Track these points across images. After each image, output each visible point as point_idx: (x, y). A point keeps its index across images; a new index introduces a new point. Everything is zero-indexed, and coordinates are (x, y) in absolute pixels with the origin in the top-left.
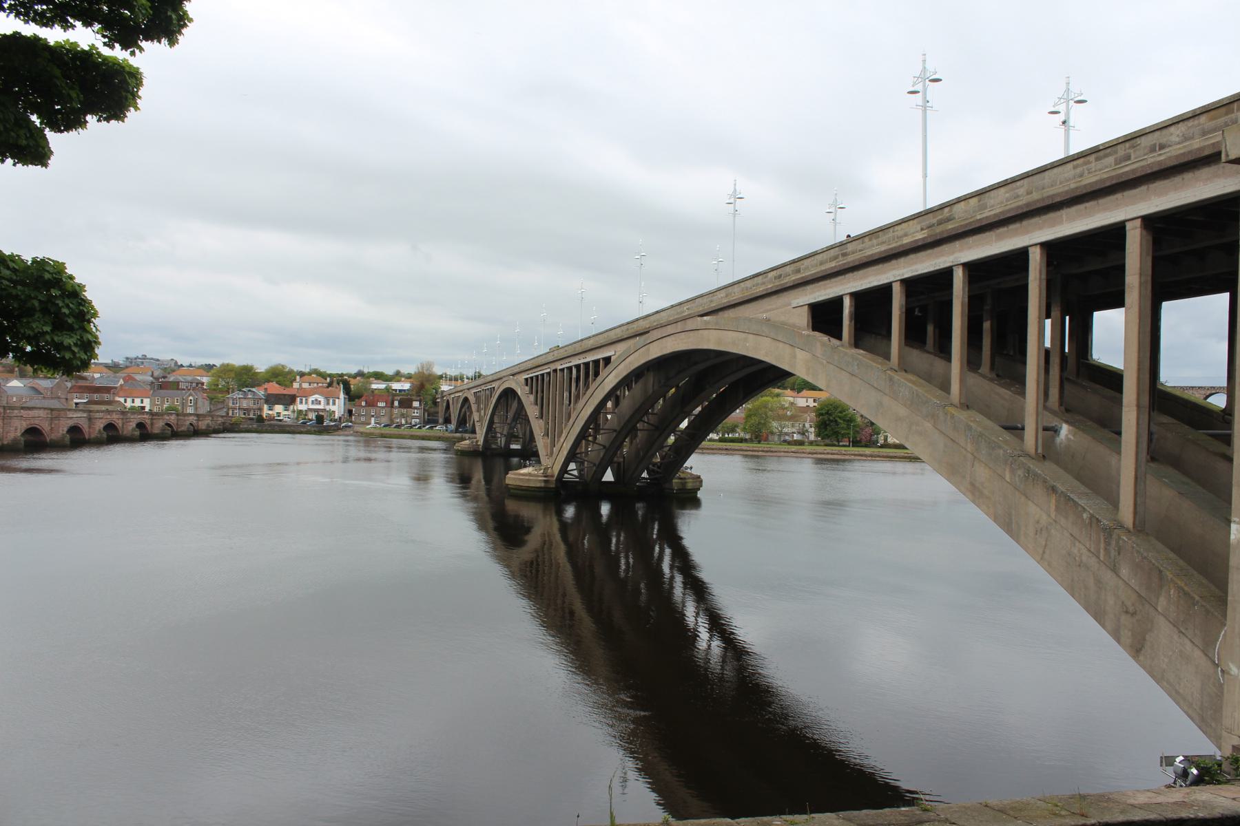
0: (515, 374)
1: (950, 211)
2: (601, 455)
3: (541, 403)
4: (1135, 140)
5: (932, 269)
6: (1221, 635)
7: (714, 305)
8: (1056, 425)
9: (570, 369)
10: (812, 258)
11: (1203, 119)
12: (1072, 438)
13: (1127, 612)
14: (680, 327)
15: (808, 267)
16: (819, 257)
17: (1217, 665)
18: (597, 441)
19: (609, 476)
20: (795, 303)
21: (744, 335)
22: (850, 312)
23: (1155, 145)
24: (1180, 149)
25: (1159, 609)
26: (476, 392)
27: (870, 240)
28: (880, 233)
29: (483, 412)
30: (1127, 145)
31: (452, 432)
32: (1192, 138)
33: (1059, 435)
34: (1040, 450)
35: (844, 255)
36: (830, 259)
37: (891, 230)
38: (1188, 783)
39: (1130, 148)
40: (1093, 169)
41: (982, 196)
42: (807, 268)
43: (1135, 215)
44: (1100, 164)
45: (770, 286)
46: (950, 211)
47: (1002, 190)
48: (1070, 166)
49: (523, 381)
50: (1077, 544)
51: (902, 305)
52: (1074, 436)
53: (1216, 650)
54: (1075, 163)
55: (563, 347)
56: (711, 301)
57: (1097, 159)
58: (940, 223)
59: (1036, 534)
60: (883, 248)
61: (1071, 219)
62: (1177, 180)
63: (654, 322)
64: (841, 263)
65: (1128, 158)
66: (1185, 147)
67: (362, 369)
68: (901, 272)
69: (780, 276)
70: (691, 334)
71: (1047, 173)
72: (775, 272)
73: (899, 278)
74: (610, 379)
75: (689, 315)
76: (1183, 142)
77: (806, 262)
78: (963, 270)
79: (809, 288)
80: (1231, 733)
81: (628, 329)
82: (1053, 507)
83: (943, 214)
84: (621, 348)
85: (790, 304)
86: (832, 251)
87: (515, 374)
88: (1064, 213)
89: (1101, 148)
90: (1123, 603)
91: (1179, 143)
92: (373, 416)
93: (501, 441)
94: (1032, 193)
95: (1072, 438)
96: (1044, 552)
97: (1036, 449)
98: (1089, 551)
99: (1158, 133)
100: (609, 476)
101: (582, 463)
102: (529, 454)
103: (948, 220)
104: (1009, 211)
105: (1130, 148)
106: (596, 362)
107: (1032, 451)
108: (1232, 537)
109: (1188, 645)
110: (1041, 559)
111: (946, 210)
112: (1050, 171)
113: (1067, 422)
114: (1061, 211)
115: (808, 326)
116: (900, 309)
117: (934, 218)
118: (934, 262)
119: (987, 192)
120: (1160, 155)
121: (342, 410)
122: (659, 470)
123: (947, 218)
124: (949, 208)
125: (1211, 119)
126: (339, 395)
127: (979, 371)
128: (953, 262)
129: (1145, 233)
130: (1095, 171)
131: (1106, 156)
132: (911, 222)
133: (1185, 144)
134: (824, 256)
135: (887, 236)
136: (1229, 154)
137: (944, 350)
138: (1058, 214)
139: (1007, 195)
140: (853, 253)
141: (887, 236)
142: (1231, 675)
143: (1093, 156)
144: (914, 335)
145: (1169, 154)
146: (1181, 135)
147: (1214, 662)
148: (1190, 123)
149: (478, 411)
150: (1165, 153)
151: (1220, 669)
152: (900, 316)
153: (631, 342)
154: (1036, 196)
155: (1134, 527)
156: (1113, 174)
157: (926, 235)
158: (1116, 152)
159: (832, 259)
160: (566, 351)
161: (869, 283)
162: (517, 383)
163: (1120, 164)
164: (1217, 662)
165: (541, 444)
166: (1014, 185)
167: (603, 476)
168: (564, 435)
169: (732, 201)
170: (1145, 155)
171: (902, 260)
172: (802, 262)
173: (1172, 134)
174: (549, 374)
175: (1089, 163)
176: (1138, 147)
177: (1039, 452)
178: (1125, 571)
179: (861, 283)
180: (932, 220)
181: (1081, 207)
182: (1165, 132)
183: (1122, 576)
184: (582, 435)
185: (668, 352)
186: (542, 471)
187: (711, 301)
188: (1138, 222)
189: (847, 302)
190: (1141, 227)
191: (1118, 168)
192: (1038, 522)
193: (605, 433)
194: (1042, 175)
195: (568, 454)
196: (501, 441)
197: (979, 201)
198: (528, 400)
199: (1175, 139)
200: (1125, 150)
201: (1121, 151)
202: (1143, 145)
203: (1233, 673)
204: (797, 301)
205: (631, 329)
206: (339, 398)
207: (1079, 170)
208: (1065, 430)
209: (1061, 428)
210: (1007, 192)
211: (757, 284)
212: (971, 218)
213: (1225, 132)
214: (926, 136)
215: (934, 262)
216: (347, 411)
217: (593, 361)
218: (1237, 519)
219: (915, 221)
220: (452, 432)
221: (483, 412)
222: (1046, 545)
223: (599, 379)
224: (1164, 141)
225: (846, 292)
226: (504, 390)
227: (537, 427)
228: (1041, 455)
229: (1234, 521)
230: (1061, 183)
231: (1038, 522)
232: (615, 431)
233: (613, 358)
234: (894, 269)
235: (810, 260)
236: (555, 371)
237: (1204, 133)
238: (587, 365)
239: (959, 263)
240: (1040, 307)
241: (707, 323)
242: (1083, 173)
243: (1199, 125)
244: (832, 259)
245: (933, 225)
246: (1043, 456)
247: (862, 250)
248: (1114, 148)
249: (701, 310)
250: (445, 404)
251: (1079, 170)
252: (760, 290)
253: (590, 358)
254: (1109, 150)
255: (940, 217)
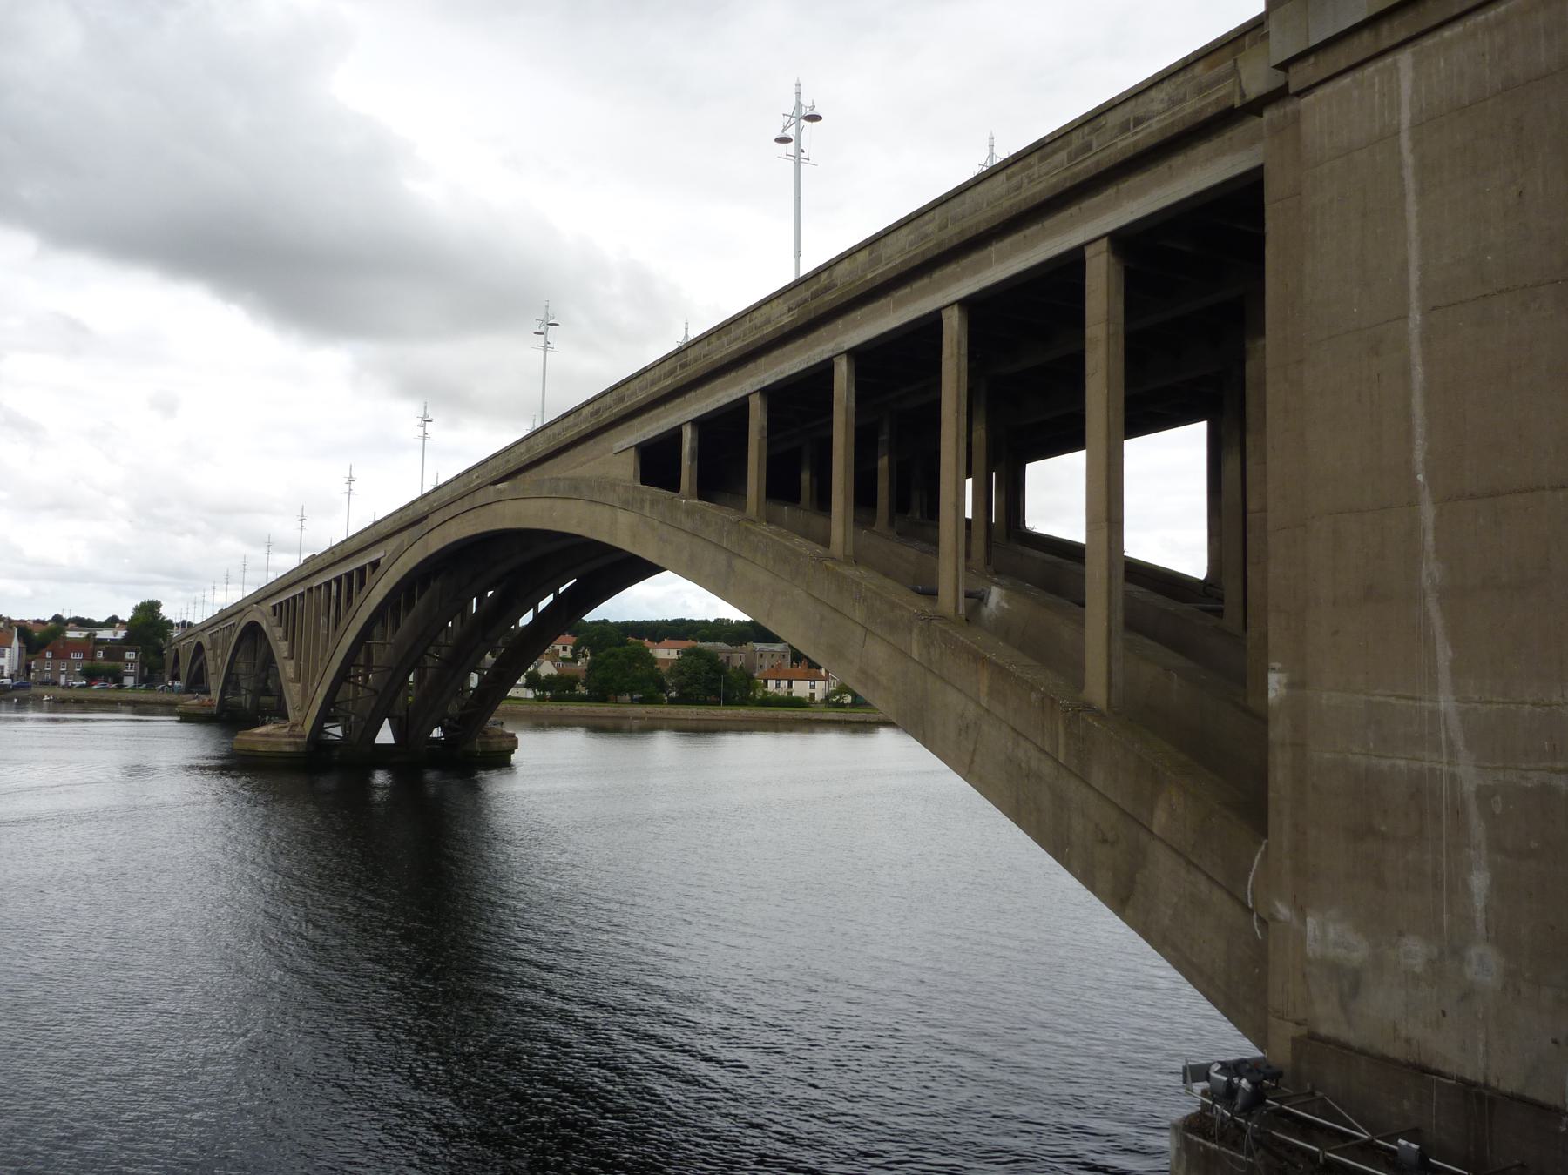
0: (261, 601)
1: (830, 276)
2: (373, 704)
3: (290, 635)
4: (1097, 120)
5: (804, 366)
6: (1256, 861)
7: (512, 466)
8: (983, 590)
9: (328, 584)
10: (641, 378)
11: (1199, 68)
12: (1006, 606)
13: (1105, 841)
14: (466, 503)
15: (635, 392)
16: (648, 375)
17: (1251, 911)
18: (368, 685)
19: (385, 736)
20: (617, 447)
21: (547, 503)
22: (691, 448)
23: (1128, 121)
24: (1165, 118)
25: (1156, 830)
26: (212, 634)
27: (719, 338)
28: (732, 326)
29: (219, 659)
30: (1086, 129)
31: (180, 692)
32: (1183, 100)
33: (986, 604)
34: (962, 610)
35: (683, 366)
36: (665, 374)
37: (748, 318)
38: (1237, 1108)
39: (1089, 134)
40: (1036, 176)
41: (873, 246)
42: (634, 393)
43: (1099, 233)
44: (1045, 167)
45: (584, 427)
46: (830, 276)
47: (904, 231)
48: (1002, 177)
49: (271, 610)
50: (1023, 742)
51: (763, 428)
52: (1008, 602)
53: (1249, 886)
54: (1009, 171)
55: (319, 555)
56: (508, 461)
57: (1042, 159)
58: (815, 296)
59: (960, 735)
60: (736, 346)
61: (1003, 258)
62: (1162, 169)
63: (435, 502)
64: (678, 378)
65: (1087, 147)
66: (1173, 114)
67: (60, 614)
68: (760, 378)
69: (597, 411)
70: (481, 511)
71: (968, 194)
72: (591, 406)
73: (758, 387)
74: (379, 591)
75: (478, 485)
76: (1169, 109)
77: (632, 385)
78: (847, 362)
79: (637, 421)
80: (1283, 1019)
81: (401, 518)
82: (984, 689)
83: (819, 281)
84: (392, 544)
85: (612, 450)
86: (667, 363)
87: (261, 601)
88: (994, 249)
89: (1048, 141)
90: (1097, 825)
91: (1164, 112)
92: (63, 672)
93: (246, 699)
94: (946, 227)
95: (1006, 606)
96: (972, 762)
97: (957, 608)
98: (1042, 750)
99: (1132, 103)
100: (385, 736)
101: (348, 719)
102: (280, 713)
103: (826, 289)
104: (911, 259)
105: (1089, 134)
106: (362, 570)
107: (950, 612)
108: (1271, 695)
109: (1204, 885)
110: (969, 772)
111: (824, 276)
112: (972, 189)
113: (996, 584)
114: (989, 248)
115: (634, 476)
116: (761, 432)
117: (807, 290)
118: (806, 356)
119: (882, 237)
120: (1137, 133)
121: (16, 664)
122: (457, 726)
123: (825, 288)
124: (828, 272)
125: (1211, 67)
126: (11, 643)
127: (874, 529)
128: (833, 351)
129: (1112, 260)
130: (1040, 177)
131: (1054, 152)
132: (776, 301)
133: (1173, 111)
134: (657, 372)
135: (742, 329)
136: (1246, 93)
137: (823, 501)
138: (984, 253)
139: (912, 237)
140: (696, 361)
141: (742, 329)
142: (1279, 922)
143: (1036, 157)
144: (781, 488)
145: (1149, 130)
146: (1167, 98)
147: (1247, 907)
148: (1180, 79)
149: (213, 660)
150: (1142, 130)
151: (1255, 916)
152: (760, 441)
153: (405, 535)
154: (953, 230)
155: (1108, 708)
156: (1067, 174)
157: (796, 316)
158: (1070, 143)
159: (666, 376)
160: (324, 559)
161: (718, 401)
162: (262, 613)
163: (1076, 158)
164: (1250, 905)
165: (292, 694)
166: (921, 221)
167: (376, 736)
168: (318, 677)
169: (542, 329)
170: (1112, 139)
171: (763, 361)
172: (627, 386)
173: (1153, 101)
174: (302, 595)
175: (1031, 166)
176: (1103, 129)
177: (960, 612)
178: (1098, 777)
179: (705, 404)
180: (805, 293)
181: (1016, 238)
182: (1142, 99)
183: (1093, 784)
184: (342, 677)
185: (452, 540)
186: (287, 730)
187: (508, 461)
188: (1104, 244)
189: (687, 434)
190: (1108, 251)
191: (1075, 165)
192: (962, 716)
193: (377, 672)
194: (961, 198)
195: (323, 703)
196: (246, 699)
197: (870, 254)
198: (275, 633)
199: (1157, 106)
200: (1083, 138)
201: (1076, 140)
202: (1109, 125)
203: (1281, 917)
204: (619, 444)
205: (406, 516)
206: (10, 647)
207: (1015, 181)
208: (996, 597)
209: (989, 593)
210: (909, 234)
211: (568, 428)
212: (860, 279)
213: (1238, 62)
214: (799, 198)
215: (806, 356)
216: (24, 666)
217: (357, 569)
218: (1277, 665)
219: (781, 300)
220: (180, 692)
221: (219, 659)
222: (974, 750)
223: (365, 591)
224: (1141, 112)
225: (686, 420)
226: (249, 623)
227: (288, 669)
228: (964, 617)
229: (1274, 669)
230: (988, 205)
231: (962, 716)
232: (390, 668)
233: (381, 562)
234: (751, 376)
235: (637, 381)
236: (310, 590)
237: (1201, 90)
238: (349, 575)
239: (842, 350)
240: (958, 396)
241: (500, 491)
242: (1022, 183)
243: (1194, 78)
244: (666, 376)
245: (806, 301)
246: (967, 620)
247: (707, 355)
248: (1066, 139)
249: (494, 475)
250: (173, 656)
251: (1015, 181)
252: (571, 434)
253: (352, 566)
254: (1058, 143)
255: (815, 288)
